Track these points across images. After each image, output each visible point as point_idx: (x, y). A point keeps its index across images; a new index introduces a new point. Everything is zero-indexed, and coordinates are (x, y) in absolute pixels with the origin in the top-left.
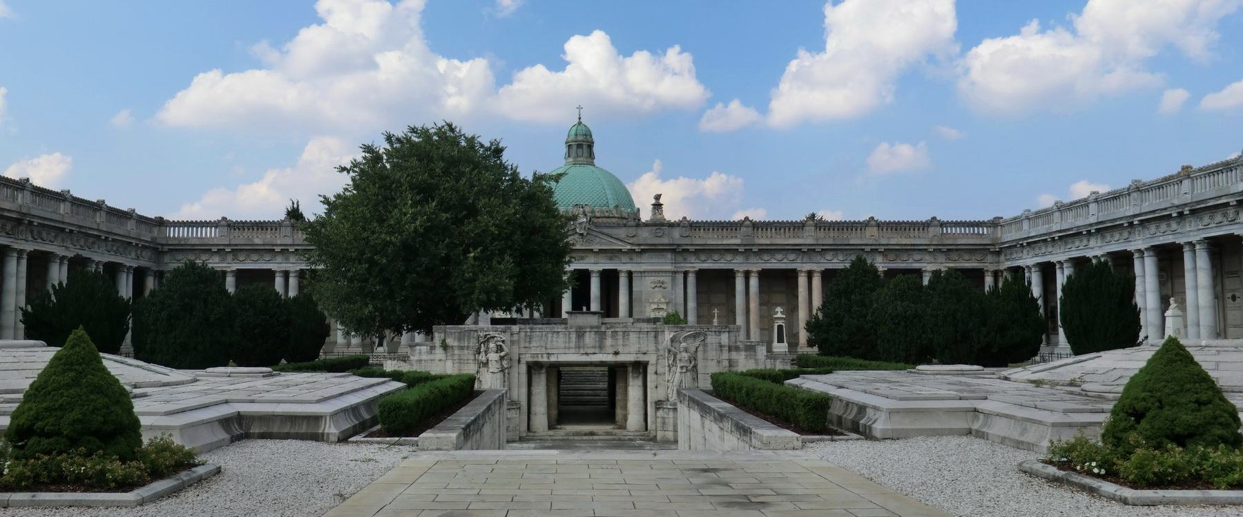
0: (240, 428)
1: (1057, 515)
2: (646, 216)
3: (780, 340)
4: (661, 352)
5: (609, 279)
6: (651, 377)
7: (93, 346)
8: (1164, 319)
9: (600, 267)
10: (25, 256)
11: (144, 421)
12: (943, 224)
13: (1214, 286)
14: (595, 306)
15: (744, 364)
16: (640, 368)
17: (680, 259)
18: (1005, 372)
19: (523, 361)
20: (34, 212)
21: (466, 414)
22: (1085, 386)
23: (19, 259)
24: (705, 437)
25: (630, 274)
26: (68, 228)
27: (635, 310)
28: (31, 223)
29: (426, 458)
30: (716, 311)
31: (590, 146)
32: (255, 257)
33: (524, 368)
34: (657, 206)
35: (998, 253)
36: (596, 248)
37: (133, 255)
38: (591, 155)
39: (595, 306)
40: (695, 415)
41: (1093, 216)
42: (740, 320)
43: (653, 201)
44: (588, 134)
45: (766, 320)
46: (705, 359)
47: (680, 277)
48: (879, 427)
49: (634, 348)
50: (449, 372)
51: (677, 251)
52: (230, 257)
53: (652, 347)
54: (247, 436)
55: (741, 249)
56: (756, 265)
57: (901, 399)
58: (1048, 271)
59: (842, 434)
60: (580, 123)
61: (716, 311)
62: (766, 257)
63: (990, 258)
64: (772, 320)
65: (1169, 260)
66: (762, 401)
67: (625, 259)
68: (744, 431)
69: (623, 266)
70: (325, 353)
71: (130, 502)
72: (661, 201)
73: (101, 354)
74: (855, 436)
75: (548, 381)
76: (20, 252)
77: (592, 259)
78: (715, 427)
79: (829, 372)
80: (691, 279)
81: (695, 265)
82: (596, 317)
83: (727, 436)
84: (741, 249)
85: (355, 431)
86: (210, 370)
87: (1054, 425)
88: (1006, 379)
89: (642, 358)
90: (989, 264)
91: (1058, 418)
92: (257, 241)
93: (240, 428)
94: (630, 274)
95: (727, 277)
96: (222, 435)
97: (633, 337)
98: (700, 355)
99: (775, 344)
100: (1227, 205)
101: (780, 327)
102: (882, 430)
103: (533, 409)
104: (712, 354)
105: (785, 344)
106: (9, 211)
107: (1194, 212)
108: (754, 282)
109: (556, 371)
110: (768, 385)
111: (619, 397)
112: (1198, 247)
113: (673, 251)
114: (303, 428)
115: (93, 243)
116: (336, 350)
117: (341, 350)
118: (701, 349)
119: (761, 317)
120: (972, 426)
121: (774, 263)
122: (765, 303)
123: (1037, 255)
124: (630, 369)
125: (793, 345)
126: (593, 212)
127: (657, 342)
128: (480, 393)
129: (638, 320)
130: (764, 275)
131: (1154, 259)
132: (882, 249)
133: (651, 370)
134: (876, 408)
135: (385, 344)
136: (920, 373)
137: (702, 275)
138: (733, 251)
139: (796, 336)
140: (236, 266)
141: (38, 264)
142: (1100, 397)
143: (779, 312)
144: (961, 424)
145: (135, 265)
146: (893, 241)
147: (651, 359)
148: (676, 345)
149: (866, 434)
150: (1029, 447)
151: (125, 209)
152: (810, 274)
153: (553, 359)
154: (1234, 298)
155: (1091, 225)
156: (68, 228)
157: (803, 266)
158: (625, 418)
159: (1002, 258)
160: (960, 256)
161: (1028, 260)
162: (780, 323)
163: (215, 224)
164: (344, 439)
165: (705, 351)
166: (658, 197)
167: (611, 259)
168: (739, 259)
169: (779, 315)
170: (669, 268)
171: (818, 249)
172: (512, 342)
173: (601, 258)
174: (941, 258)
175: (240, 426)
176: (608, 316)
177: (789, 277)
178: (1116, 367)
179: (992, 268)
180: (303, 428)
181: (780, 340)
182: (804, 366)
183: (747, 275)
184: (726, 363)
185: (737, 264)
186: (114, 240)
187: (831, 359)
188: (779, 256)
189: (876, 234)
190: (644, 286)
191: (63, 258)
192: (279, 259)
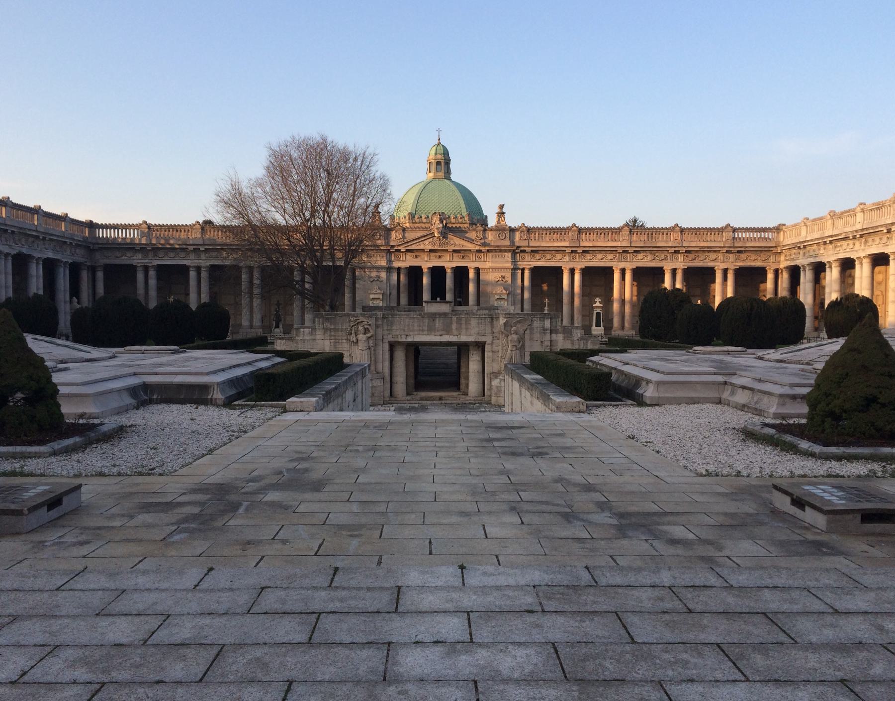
0: (147, 395)
2: (492, 222)
3: (598, 325)
4: (496, 335)
7: (20, 330)
11: (63, 390)
12: (735, 230)
14: (449, 296)
15: (562, 343)
16: (481, 346)
18: (760, 353)
19: (386, 341)
21: (329, 384)
24: (523, 404)
25: (478, 270)
26: (10, 230)
31: (447, 162)
33: (387, 347)
34: (501, 214)
38: (448, 172)
40: (516, 384)
41: (859, 222)
42: (566, 309)
43: (498, 210)
44: (446, 153)
46: (531, 339)
47: (519, 272)
48: (649, 392)
49: (474, 331)
50: (327, 349)
51: (516, 251)
52: (151, 255)
53: (488, 330)
54: (151, 402)
57: (669, 374)
59: (620, 400)
60: (439, 144)
68: (546, 399)
70: (233, 333)
71: (44, 453)
72: (504, 210)
73: (25, 335)
74: (630, 402)
75: (407, 356)
78: (528, 394)
79: (625, 351)
81: (529, 263)
83: (536, 401)
85: (239, 396)
86: (128, 348)
87: (781, 396)
88: (761, 358)
89: (482, 339)
91: (787, 390)
93: (147, 395)
94: (478, 270)
96: (128, 400)
97: (474, 322)
98: (527, 337)
99: (594, 327)
101: (598, 314)
102: (651, 398)
104: (537, 336)
109: (414, 350)
111: (463, 370)
114: (194, 395)
115: (33, 242)
116: (241, 331)
118: (528, 332)
120: (716, 393)
121: (597, 262)
124: (471, 348)
125: (608, 328)
127: (492, 327)
128: (348, 365)
129: (482, 309)
134: (648, 382)
135: (281, 326)
136: (695, 352)
139: (611, 321)
143: (598, 303)
144: (713, 394)
145: (70, 261)
147: (488, 339)
148: (508, 328)
149: (640, 402)
150: (759, 412)
151: (59, 214)
153: (410, 339)
155: (856, 231)
156: (10, 230)
158: (467, 386)
162: (599, 310)
163: (138, 227)
164: (228, 403)
165: (531, 333)
166: (502, 207)
169: (598, 304)
172: (377, 326)
175: (146, 393)
179: (775, 266)
180: (194, 395)
181: (598, 325)
182: (621, 345)
184: (548, 343)
186: (51, 240)
188: (600, 256)
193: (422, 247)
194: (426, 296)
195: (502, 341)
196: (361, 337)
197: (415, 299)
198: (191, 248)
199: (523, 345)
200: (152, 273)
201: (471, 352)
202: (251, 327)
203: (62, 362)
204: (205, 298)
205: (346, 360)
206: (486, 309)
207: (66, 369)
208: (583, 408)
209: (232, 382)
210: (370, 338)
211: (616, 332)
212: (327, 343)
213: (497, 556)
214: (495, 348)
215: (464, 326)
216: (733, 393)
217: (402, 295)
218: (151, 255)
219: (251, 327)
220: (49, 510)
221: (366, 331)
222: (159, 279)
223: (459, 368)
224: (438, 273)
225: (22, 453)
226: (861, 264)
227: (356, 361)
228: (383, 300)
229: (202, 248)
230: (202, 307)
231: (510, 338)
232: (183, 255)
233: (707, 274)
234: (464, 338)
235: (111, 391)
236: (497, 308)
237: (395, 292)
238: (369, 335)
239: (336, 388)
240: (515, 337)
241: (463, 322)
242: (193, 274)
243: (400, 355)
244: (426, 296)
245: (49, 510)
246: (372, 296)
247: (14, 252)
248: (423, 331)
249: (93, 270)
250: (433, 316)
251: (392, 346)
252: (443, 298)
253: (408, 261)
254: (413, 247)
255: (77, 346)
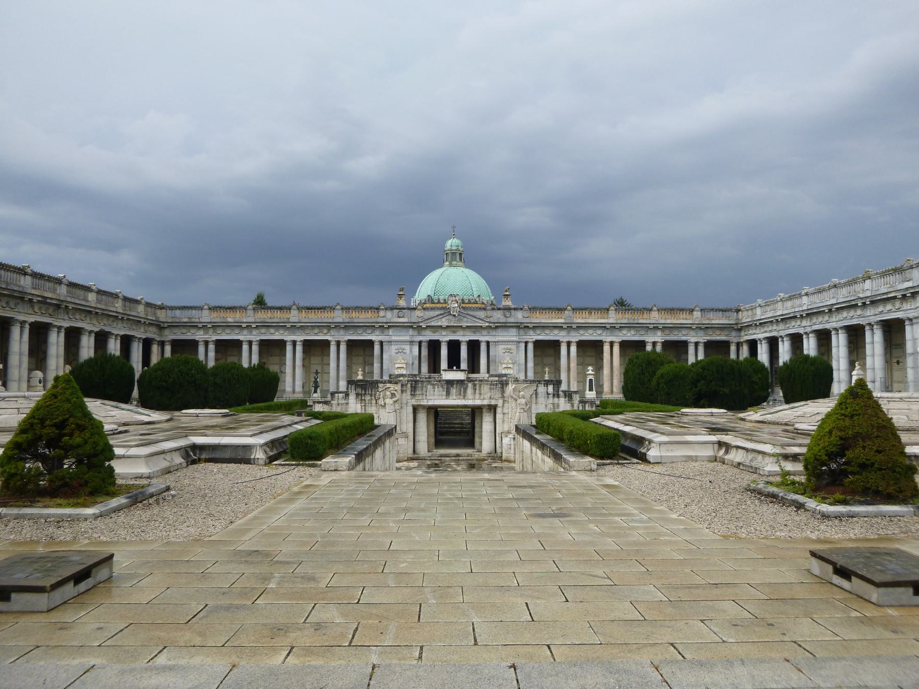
1: (915, 407)
5: (474, 346)
6: (499, 416)
8: (851, 376)
9: (448, 339)
10: (63, 330)
13: (886, 354)
14: (464, 365)
16: (493, 409)
17: (522, 332)
20: (69, 299)
21: (361, 444)
22: (797, 426)
23: (58, 332)
25: (488, 343)
27: (491, 368)
28: (67, 307)
29: (325, 479)
30: (547, 369)
32: (228, 331)
33: (410, 409)
35: (740, 330)
36: (464, 325)
37: (142, 330)
39: (464, 365)
45: (582, 375)
50: (359, 411)
52: (211, 331)
53: (498, 395)
54: (199, 461)
55: (565, 326)
56: (575, 337)
58: (773, 343)
61: (547, 369)
62: (582, 332)
63: (734, 333)
64: (586, 375)
65: (856, 335)
66: (570, 436)
67: (485, 332)
68: (557, 457)
69: (482, 338)
73: (86, 399)
74: (635, 461)
76: (59, 328)
77: (461, 332)
78: (539, 453)
80: (531, 346)
82: (463, 373)
84: (565, 326)
89: (493, 402)
90: (733, 338)
91: (778, 450)
92: (230, 320)
94: (488, 343)
95: (555, 345)
97: (486, 388)
99: (587, 392)
100: (895, 298)
101: (591, 380)
102: (654, 457)
103: (417, 438)
105: (594, 392)
106: (51, 299)
107: (873, 302)
108: (573, 349)
109: (435, 412)
110: (581, 424)
111: (477, 430)
112: (875, 327)
113: (518, 327)
117: (288, 396)
119: (578, 373)
121: (588, 336)
122: (582, 364)
123: (766, 332)
124: (484, 410)
125: (599, 393)
126: (463, 300)
128: (378, 426)
129: (492, 376)
130: (581, 344)
131: (845, 335)
132: (661, 327)
133: (499, 410)
135: (318, 391)
137: (538, 344)
138: (559, 327)
139: (602, 386)
140: (215, 338)
141: (73, 337)
142: (805, 434)
146: (669, 321)
149: (643, 458)
150: (755, 470)
152: (612, 344)
153: (431, 403)
154: (898, 363)
157: (607, 338)
159: (743, 333)
160: (224, 330)
161: (759, 334)
167: (474, 333)
168: (563, 333)
169: (590, 372)
170: (407, 338)
171: (618, 326)
172: (402, 391)
173: (468, 332)
174: (701, 333)
176: (473, 372)
177: (597, 346)
178: (811, 414)
179: (735, 340)
180: (240, 456)
182: (606, 408)
183: (569, 344)
185: (607, 338)
186: (128, 319)
187: (631, 403)
188: (590, 331)
189: (657, 316)
190: (498, 351)
191: (90, 332)
192: (245, 332)
193: (439, 324)
194: (444, 364)
195: (512, 404)
196: (389, 401)
197: (434, 367)
198: (244, 325)
199: (530, 408)
200: (212, 347)
201: (484, 414)
202: (294, 392)
203: (124, 424)
204: (255, 360)
205: (376, 422)
206: (496, 376)
207: (126, 432)
208: (594, 467)
209: (272, 443)
210: (395, 402)
211: (606, 396)
212: (359, 406)
213: (548, 646)
214: (506, 411)
215: (477, 391)
216: (727, 452)
217: (423, 365)
218: (211, 331)
219: (294, 392)
220: (75, 585)
221: (393, 395)
222: (217, 351)
223: (473, 428)
224: (454, 346)
225: (70, 516)
226: (808, 338)
227: (382, 422)
228: (406, 369)
229: (254, 326)
230: (252, 369)
231: (519, 401)
232: (237, 331)
233: (682, 346)
234: (478, 402)
235: (163, 452)
236: (505, 375)
237: (417, 362)
238: (395, 399)
239: (367, 448)
240: (523, 401)
241: (478, 387)
242: (245, 347)
243: (422, 417)
244: (444, 364)
245: (75, 585)
246: (397, 366)
247: (96, 330)
248: (442, 395)
249: (162, 344)
250: (450, 383)
251: (415, 409)
252: (458, 367)
253: (428, 336)
254: (433, 324)
255: (141, 410)
